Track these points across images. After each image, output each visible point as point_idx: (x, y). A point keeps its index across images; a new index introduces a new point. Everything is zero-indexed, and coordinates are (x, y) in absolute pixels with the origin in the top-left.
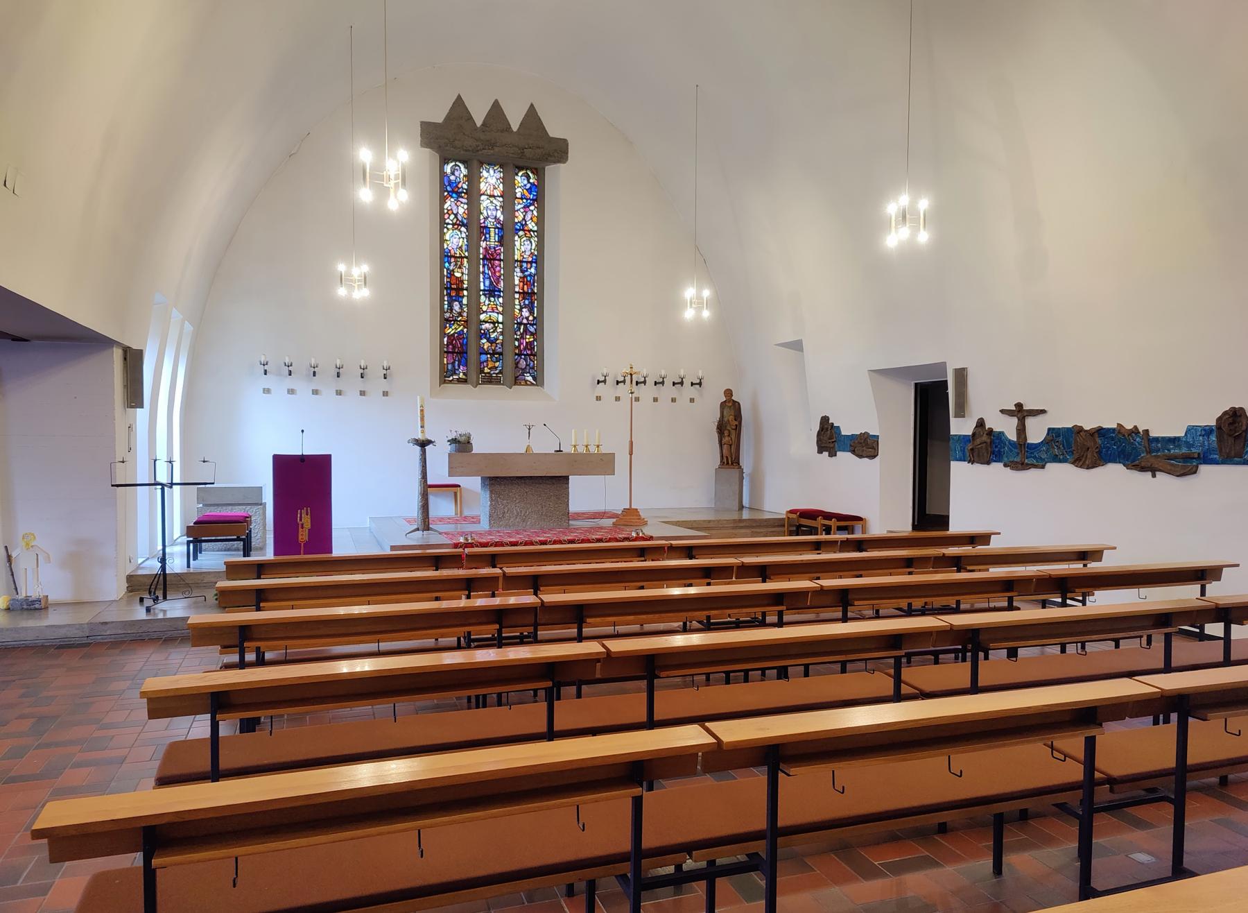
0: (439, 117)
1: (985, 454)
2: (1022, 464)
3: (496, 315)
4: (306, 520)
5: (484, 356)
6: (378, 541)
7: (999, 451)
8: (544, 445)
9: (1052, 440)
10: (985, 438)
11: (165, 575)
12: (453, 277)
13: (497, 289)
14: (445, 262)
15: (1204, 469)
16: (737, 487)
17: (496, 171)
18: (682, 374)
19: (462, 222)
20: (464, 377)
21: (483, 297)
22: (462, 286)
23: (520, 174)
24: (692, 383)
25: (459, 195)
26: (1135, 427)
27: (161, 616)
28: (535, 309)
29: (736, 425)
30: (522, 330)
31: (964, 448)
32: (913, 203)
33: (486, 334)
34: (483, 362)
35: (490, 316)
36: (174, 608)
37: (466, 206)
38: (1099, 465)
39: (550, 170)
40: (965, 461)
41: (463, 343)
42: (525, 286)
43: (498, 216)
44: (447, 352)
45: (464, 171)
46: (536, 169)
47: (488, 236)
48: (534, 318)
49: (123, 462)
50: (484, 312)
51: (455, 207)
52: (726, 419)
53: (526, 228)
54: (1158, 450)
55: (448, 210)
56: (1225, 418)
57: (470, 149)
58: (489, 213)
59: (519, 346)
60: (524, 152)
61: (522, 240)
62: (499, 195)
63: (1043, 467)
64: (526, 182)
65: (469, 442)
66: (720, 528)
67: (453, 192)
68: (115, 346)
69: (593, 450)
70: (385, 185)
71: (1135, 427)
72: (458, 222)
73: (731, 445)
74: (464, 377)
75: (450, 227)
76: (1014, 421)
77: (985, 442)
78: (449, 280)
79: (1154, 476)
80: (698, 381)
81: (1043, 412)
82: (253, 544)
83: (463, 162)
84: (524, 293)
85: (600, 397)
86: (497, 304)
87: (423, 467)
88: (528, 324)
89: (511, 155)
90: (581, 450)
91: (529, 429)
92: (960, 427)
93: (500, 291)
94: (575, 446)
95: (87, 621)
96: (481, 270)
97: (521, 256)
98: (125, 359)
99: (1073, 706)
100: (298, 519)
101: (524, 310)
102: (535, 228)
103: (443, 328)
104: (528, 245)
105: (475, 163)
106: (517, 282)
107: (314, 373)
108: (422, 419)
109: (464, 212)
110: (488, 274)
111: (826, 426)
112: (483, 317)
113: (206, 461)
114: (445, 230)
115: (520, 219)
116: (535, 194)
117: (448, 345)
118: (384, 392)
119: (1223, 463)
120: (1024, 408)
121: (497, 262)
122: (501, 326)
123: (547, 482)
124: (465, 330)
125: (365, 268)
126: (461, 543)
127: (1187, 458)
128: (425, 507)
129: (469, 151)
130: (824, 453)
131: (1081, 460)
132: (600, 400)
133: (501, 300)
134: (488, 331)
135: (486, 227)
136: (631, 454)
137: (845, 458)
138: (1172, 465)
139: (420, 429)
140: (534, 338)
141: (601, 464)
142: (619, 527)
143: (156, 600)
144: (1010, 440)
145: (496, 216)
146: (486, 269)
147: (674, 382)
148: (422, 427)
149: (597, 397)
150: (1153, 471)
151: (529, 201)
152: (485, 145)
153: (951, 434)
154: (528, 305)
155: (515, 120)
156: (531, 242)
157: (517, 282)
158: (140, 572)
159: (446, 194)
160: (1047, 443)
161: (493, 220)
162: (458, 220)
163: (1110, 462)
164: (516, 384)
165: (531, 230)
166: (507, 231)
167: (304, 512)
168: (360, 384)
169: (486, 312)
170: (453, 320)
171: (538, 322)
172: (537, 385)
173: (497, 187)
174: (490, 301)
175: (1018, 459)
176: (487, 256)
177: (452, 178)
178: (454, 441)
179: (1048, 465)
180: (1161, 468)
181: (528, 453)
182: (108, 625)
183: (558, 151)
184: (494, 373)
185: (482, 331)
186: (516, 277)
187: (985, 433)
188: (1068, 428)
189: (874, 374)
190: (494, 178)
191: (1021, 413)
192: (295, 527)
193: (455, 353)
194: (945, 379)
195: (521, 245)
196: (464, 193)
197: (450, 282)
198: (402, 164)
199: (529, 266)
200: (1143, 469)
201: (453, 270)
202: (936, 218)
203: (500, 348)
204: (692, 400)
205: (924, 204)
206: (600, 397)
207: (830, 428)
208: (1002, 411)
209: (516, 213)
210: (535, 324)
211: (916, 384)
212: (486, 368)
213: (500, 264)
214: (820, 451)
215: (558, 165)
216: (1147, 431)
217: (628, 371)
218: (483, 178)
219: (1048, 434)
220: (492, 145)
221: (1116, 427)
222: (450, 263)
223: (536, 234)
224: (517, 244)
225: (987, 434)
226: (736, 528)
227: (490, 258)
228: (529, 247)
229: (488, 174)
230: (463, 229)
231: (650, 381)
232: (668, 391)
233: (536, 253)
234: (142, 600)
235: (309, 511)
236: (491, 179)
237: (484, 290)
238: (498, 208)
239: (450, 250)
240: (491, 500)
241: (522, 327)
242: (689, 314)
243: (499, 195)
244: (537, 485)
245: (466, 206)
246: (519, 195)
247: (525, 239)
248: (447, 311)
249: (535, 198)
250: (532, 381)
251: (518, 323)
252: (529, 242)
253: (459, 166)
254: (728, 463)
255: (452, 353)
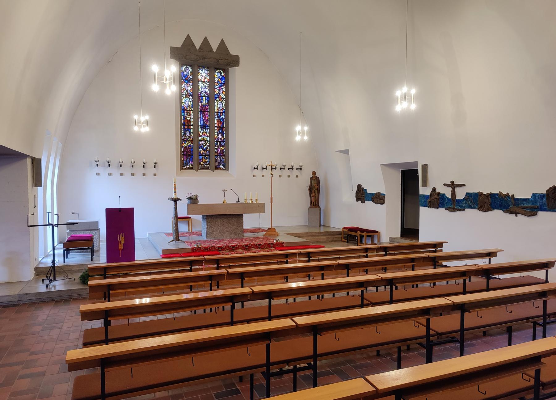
0: (179, 44)
1: (436, 204)
2: (454, 209)
3: (206, 137)
4: (122, 240)
5: (201, 156)
6: (153, 246)
7: (443, 202)
8: (231, 200)
9: (468, 198)
10: (436, 196)
11: (54, 266)
12: (186, 120)
13: (206, 125)
14: (182, 113)
15: (540, 213)
16: (318, 217)
17: (206, 70)
18: (293, 165)
19: (190, 94)
20: (192, 166)
21: (200, 129)
22: (190, 124)
23: (217, 72)
24: (297, 168)
25: (188, 81)
26: (508, 193)
27: (53, 290)
28: (225, 134)
29: (318, 188)
30: (218, 144)
31: (426, 201)
32: (409, 91)
33: (202, 146)
34: (200, 160)
35: (204, 138)
36: (59, 285)
37: (192, 87)
38: (491, 210)
39: (231, 70)
40: (426, 206)
41: (191, 150)
42: (220, 124)
43: (207, 91)
44: (184, 155)
45: (191, 70)
46: (224, 69)
47: (202, 100)
48: (224, 139)
49: (33, 214)
50: (201, 136)
51: (187, 87)
52: (313, 185)
53: (220, 97)
54: (519, 204)
55: (184, 88)
56: (550, 190)
57: (194, 60)
58: (203, 90)
59: (217, 152)
60: (219, 62)
61: (218, 103)
62: (207, 81)
63: (464, 210)
64: (219, 75)
65: (197, 199)
66: (312, 236)
67: (186, 80)
68: (28, 157)
69: (254, 201)
70: (165, 83)
71: (508, 193)
72: (188, 94)
73: (315, 197)
74: (192, 166)
75: (184, 96)
76: (450, 189)
77: (436, 198)
78: (184, 121)
79: (516, 216)
80: (300, 168)
81: (464, 185)
82: (94, 249)
83: (189, 66)
84: (219, 127)
85: (255, 175)
86: (206, 133)
87: (176, 211)
88: (221, 141)
89: (213, 63)
90: (249, 201)
91: (225, 192)
92: (424, 191)
93: (208, 126)
94: (246, 200)
95: (17, 293)
96: (199, 116)
97: (218, 110)
98: (32, 163)
99: (534, 355)
100: (118, 239)
101: (219, 135)
102: (224, 97)
103: (182, 144)
104: (221, 104)
105: (196, 67)
106: (216, 122)
107: (121, 165)
108: (175, 188)
109: (191, 89)
110: (203, 118)
111: (360, 189)
112: (200, 138)
113: (74, 213)
114: (182, 98)
115: (217, 93)
116: (224, 81)
117: (184, 151)
118: (154, 174)
119: (549, 210)
120: (455, 183)
121: (206, 113)
122: (208, 142)
123: (233, 216)
124: (192, 144)
125: (147, 117)
126: (195, 247)
127: (532, 208)
128: (177, 230)
129: (193, 61)
130: (359, 201)
131: (482, 208)
132: (255, 177)
133: (208, 130)
134: (203, 145)
135: (201, 96)
136: (272, 203)
137: (369, 204)
138: (525, 211)
139: (174, 193)
140: (224, 148)
141: (258, 208)
142: (267, 237)
143: (50, 281)
144: (448, 198)
145: (206, 91)
146: (201, 116)
147: (289, 168)
148: (175, 192)
149: (254, 175)
150: (516, 214)
151: (221, 84)
152: (201, 58)
153: (420, 194)
154: (221, 133)
155: (214, 47)
156: (222, 103)
157: (216, 122)
158: (41, 266)
159: (182, 80)
160: (466, 199)
161: (205, 93)
162: (188, 93)
163: (495, 209)
164: (216, 169)
165: (222, 98)
166: (211, 98)
167: (121, 235)
168: (143, 171)
169: (201, 136)
170: (186, 140)
171: (226, 140)
172: (225, 170)
173: (206, 77)
174: (203, 131)
175: (452, 206)
176: (202, 110)
177: (185, 73)
178: (190, 198)
179: (466, 210)
180: (520, 212)
181: (224, 204)
182: (28, 295)
183: (235, 61)
184: (206, 165)
185: (200, 145)
186: (215, 120)
187: (436, 194)
188: (475, 193)
189: (381, 165)
190: (205, 73)
191: (453, 186)
192: (117, 243)
193: (187, 155)
194: (417, 169)
195: (217, 105)
196: (191, 80)
197: (184, 122)
198: (173, 73)
199: (221, 114)
200: (511, 213)
201: (186, 116)
202: (417, 98)
203: (208, 153)
204: (297, 176)
205: (413, 91)
206: (255, 175)
207: (362, 190)
208: (444, 185)
209: (215, 90)
210: (225, 142)
211: (402, 170)
212: (202, 162)
213: (208, 114)
214: (357, 200)
215: (235, 67)
216: (513, 195)
217: (270, 164)
218: (200, 73)
219: (466, 195)
220: (204, 58)
221: (498, 193)
222: (184, 113)
223: (224, 99)
224: (216, 104)
225: (437, 195)
226: (318, 236)
227: (203, 111)
228: (221, 106)
229: (202, 71)
230: (190, 97)
231: (278, 168)
232: (286, 172)
233: (225, 109)
234: (43, 280)
235: (124, 235)
236: (203, 74)
237: (201, 126)
238: (207, 87)
239: (184, 107)
240: (207, 226)
241: (218, 143)
242: (298, 138)
243: (207, 81)
244: (228, 218)
245: (192, 87)
246: (216, 81)
247: (219, 102)
248: (184, 136)
249: (224, 83)
250: (223, 168)
251: (216, 141)
252: (221, 103)
253: (188, 68)
254: (314, 205)
255: (186, 155)
